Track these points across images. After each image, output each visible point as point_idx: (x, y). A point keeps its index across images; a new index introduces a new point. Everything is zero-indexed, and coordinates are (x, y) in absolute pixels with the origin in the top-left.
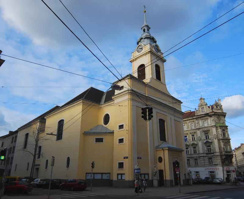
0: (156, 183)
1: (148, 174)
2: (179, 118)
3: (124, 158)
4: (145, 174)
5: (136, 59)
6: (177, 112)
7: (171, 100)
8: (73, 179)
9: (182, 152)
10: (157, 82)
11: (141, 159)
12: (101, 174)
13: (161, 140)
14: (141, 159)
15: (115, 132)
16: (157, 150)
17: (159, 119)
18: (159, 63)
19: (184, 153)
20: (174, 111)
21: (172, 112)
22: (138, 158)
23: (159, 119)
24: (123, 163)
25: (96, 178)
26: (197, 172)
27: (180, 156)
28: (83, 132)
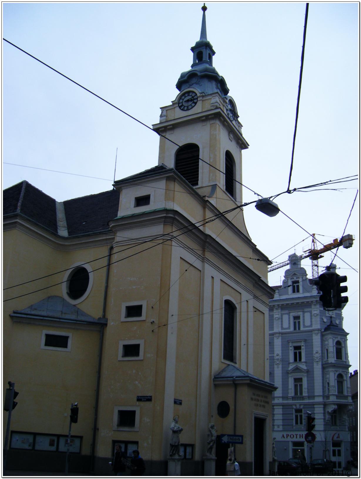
4: (185, 446)
5: (173, 125)
6: (260, 286)
7: (250, 253)
13: (225, 357)
14: (181, 404)
19: (278, 393)
20: (256, 283)
22: (175, 402)
24: (133, 413)
25: (63, 448)
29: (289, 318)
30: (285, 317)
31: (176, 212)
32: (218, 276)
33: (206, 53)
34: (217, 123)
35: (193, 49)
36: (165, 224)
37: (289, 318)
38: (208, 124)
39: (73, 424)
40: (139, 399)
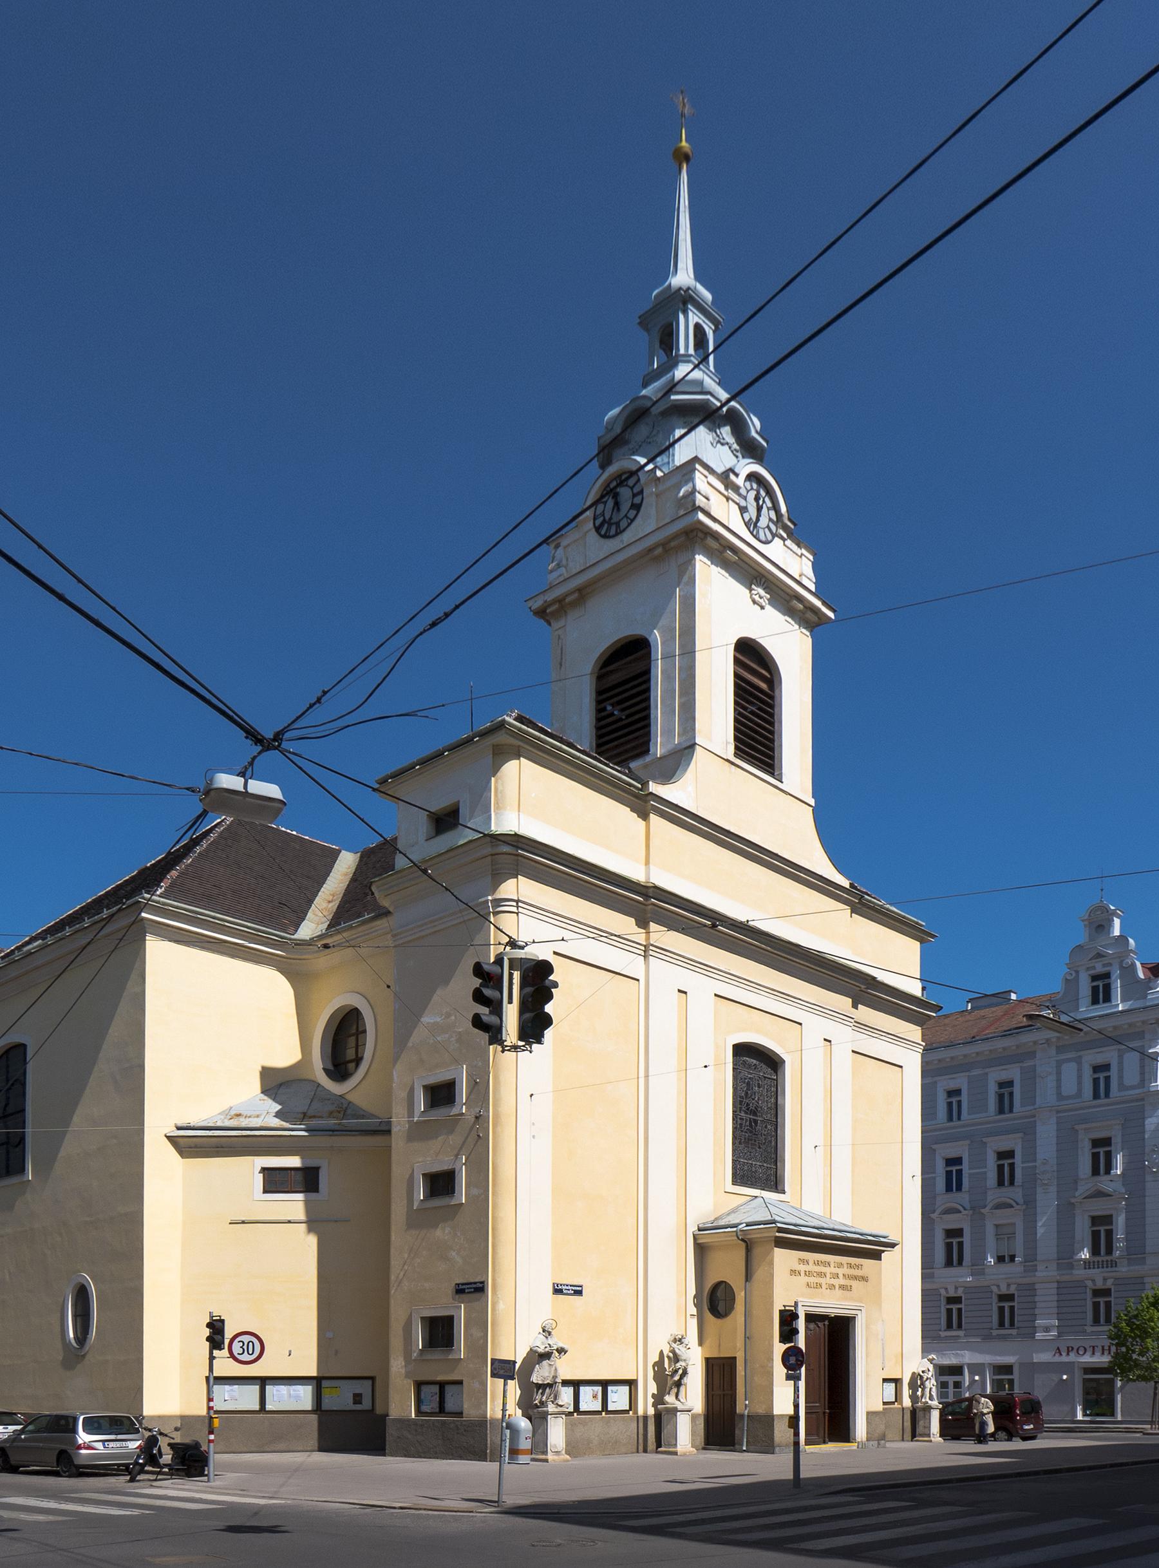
3: (557, 1291)
9: (877, 1256)
10: (747, 781)
11: (579, 1293)
12: (893, 1385)
13: (742, 1176)
15: (394, 1130)
22: (557, 1291)
27: (864, 1279)
29: (1080, 1070)
30: (1070, 1070)
32: (702, 987)
37: (1080, 1070)
39: (216, 1353)
40: (460, 1290)
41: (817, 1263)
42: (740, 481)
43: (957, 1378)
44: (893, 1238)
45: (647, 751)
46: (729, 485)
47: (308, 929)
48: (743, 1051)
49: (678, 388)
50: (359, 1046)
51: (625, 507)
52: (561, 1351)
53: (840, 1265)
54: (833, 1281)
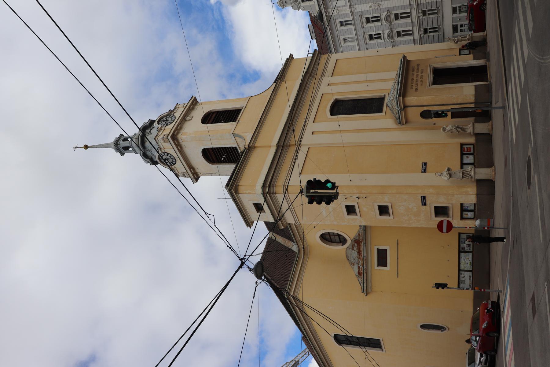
0: (482, 128)
1: (462, 145)
2: (327, 63)
5: (190, 169)
8: (489, 53)
9: (409, 62)
10: (243, 117)
11: (425, 164)
13: (380, 110)
15: (363, 224)
16: (406, 122)
17: (332, 114)
18: (199, 114)
20: (310, 75)
21: (312, 83)
22: (425, 171)
23: (332, 113)
26: (454, 10)
27: (418, 65)
28: (363, 295)
31: (264, 186)
32: (311, 127)
33: (123, 144)
34: (181, 137)
35: (122, 154)
36: (274, 193)
38: (182, 143)
39: (448, 286)
41: (412, 82)
42: (160, 126)
43: (459, 26)
44: (402, 57)
45: (236, 148)
46: (161, 129)
47: (295, 248)
48: (332, 113)
49: (137, 144)
50: (334, 234)
51: (168, 157)
52: (449, 170)
53: (413, 74)
54: (419, 76)
